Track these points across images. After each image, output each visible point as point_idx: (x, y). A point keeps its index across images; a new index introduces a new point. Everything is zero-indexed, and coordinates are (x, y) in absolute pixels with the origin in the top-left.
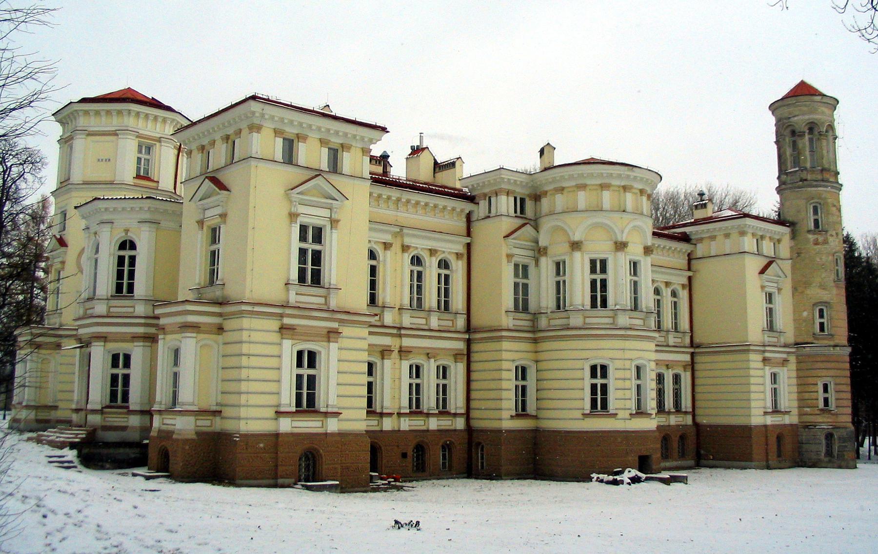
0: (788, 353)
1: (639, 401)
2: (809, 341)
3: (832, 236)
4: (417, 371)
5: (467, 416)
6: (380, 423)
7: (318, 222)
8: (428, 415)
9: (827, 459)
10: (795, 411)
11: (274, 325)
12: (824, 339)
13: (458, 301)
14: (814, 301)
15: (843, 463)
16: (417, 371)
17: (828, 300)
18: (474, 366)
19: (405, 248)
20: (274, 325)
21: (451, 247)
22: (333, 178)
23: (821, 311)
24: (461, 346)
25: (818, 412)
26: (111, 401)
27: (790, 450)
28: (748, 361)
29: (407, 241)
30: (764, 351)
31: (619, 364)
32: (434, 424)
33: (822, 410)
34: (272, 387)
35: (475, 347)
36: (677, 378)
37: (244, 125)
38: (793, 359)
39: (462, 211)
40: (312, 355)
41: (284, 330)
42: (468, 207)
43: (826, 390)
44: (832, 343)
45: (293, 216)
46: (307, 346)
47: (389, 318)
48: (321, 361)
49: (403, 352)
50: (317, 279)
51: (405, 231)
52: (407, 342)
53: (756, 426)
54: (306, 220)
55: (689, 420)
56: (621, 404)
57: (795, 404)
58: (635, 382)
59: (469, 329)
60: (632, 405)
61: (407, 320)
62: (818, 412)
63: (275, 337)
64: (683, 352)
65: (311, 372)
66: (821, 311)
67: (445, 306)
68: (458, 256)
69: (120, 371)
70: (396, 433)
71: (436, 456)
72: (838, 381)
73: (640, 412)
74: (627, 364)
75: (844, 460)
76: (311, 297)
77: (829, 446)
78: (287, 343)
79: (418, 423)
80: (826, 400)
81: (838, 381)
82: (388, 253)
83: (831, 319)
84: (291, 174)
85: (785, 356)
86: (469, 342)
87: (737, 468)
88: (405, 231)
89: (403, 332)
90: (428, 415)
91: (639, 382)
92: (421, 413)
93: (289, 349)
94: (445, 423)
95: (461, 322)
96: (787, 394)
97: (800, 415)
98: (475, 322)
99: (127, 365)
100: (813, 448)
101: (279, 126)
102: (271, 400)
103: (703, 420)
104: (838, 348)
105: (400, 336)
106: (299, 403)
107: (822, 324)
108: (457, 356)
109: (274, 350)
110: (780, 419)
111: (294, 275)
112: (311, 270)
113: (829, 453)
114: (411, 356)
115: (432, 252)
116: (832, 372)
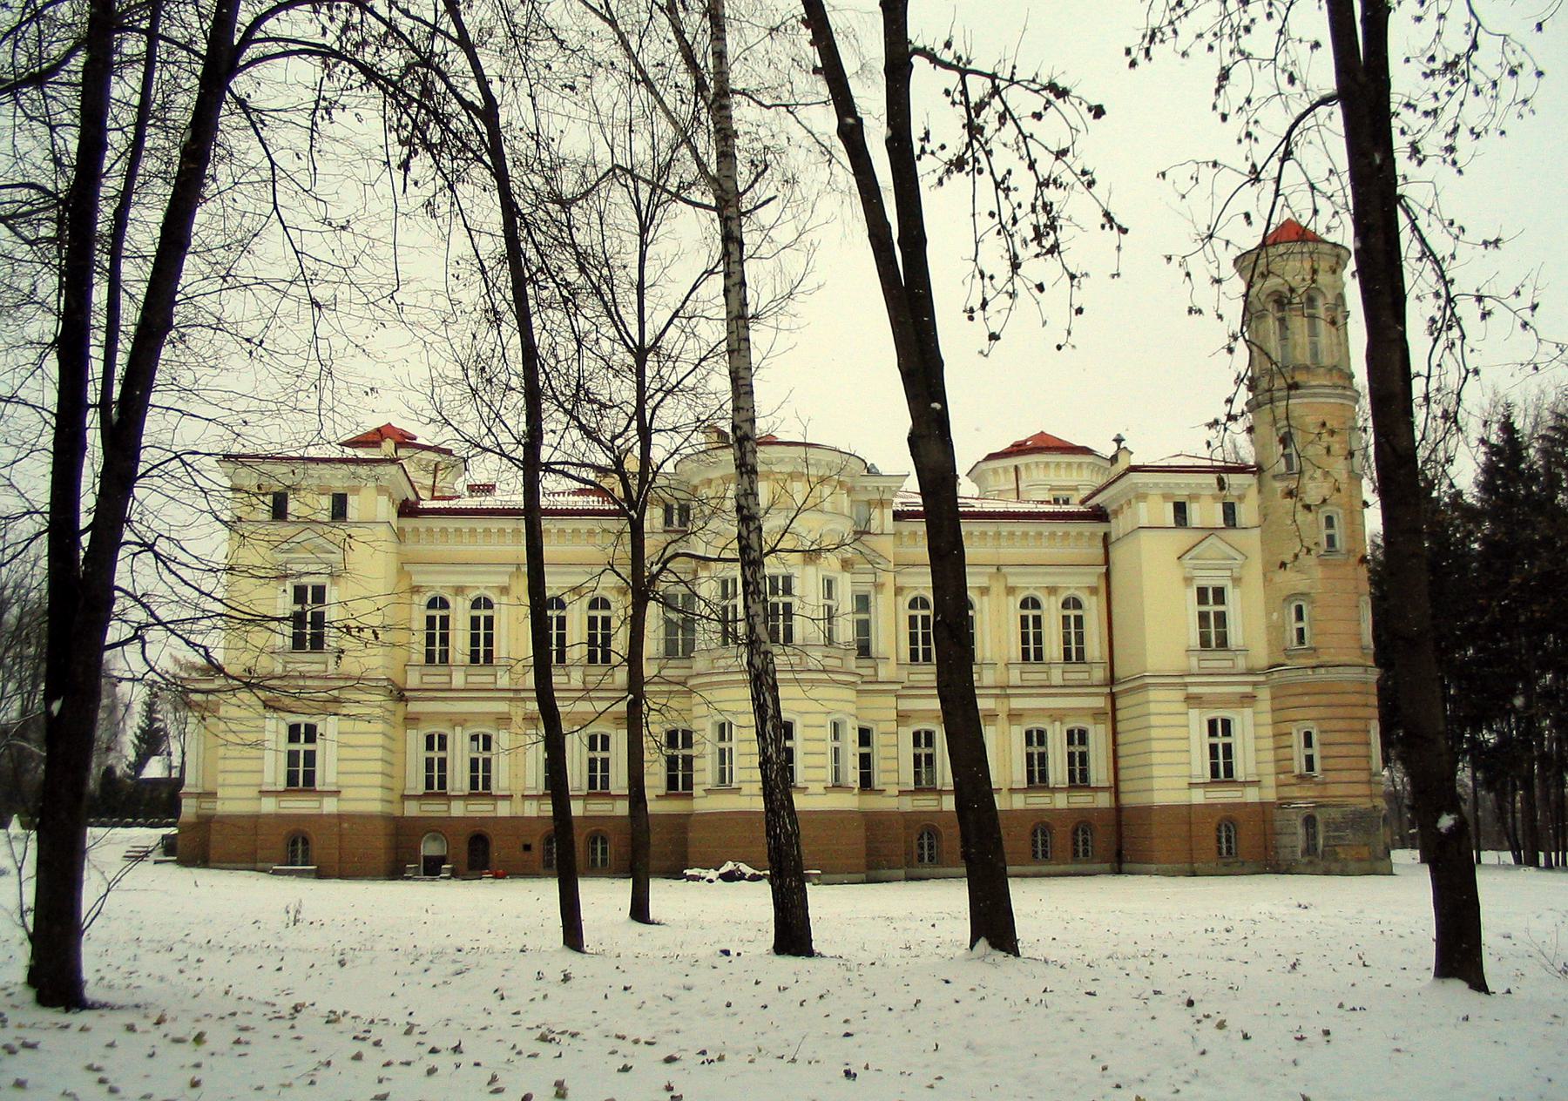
0: (1255, 684)
1: (837, 770)
2: (1281, 661)
3: (1312, 478)
4: (435, 742)
5: (1116, 789)
6: (940, 803)
7: (1218, 583)
8: (1054, 790)
9: (1305, 860)
10: (1270, 781)
11: (1179, 695)
12: (1300, 656)
13: (1094, 647)
14: (1285, 593)
15: (1334, 867)
16: (435, 742)
17: (1305, 590)
18: (1120, 727)
19: (1011, 591)
20: (1179, 695)
21: (1077, 583)
22: (1231, 535)
23: (1299, 610)
24: (1100, 702)
25: (1294, 781)
26: (289, 784)
27: (1237, 843)
28: (1148, 702)
29: (1012, 581)
30: (1186, 685)
31: (809, 719)
32: (1061, 801)
33: (1300, 777)
34: (1182, 757)
35: (1120, 703)
36: (1078, 737)
37: (1131, 496)
38: (1264, 694)
39: (1093, 535)
40: (1227, 724)
41: (1193, 700)
42: (1100, 528)
43: (1308, 744)
44: (1313, 662)
45: (1188, 580)
46: (1219, 714)
47: (885, 672)
48: (1236, 728)
49: (1014, 716)
50: (1223, 642)
51: (1004, 570)
52: (1016, 703)
53: (1165, 808)
54: (1203, 583)
55: (622, 808)
56: (812, 774)
57: (1270, 768)
58: (830, 744)
59: (1112, 680)
60: (828, 775)
61: (1015, 676)
62: (1294, 781)
63: (1182, 707)
64: (1097, 694)
65: (1227, 740)
66: (1299, 610)
67: (1074, 654)
68: (1093, 591)
69: (599, 755)
70: (515, 821)
71: (1061, 838)
72: (1327, 725)
73: (838, 785)
74: (820, 719)
75: (1336, 860)
76: (1216, 661)
77: (1311, 836)
78: (1194, 713)
79: (1039, 801)
80: (1309, 759)
81: (1327, 725)
82: (985, 598)
83: (1312, 620)
84: (1183, 538)
85: (1248, 689)
86: (1113, 697)
87: (1035, 876)
88: (1004, 570)
89: (1009, 691)
90: (1054, 790)
91: (836, 744)
92: (609, 795)
93: (1197, 721)
94: (1082, 800)
95: (1099, 674)
96: (1193, 750)
97: (1279, 785)
98: (1118, 673)
99: (605, 747)
100: (1285, 840)
101: (1166, 491)
102: (1183, 770)
103: (1128, 800)
104: (1323, 670)
105: (1008, 696)
106: (429, 785)
107: (1301, 632)
108: (1097, 714)
109: (1181, 720)
110: (1090, 799)
111: (1195, 641)
112: (1214, 632)
113: (1310, 849)
114: (911, 721)
115: (1052, 590)
116: (1314, 713)
